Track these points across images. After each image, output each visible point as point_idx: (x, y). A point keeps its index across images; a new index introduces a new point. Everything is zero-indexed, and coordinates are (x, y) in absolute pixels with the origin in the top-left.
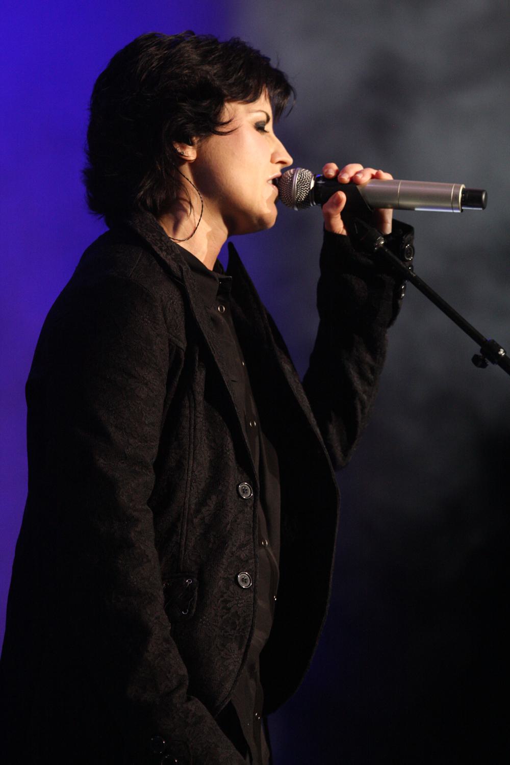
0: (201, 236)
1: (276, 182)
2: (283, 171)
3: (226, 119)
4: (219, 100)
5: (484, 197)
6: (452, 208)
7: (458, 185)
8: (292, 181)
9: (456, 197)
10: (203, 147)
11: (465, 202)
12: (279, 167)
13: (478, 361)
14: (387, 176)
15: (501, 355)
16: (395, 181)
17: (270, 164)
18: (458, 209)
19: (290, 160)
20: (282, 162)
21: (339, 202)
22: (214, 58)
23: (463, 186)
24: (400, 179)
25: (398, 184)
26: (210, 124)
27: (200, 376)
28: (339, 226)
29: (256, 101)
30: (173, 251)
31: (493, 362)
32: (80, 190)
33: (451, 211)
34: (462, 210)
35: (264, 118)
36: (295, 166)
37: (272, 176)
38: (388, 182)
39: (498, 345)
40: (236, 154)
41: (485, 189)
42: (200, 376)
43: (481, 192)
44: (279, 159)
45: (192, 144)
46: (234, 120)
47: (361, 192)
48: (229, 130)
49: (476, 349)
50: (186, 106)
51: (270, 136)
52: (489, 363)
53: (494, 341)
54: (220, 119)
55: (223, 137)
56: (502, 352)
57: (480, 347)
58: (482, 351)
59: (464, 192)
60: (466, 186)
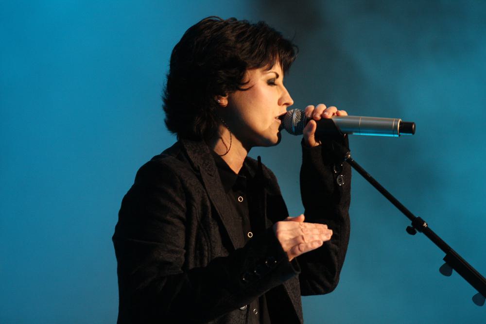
0: (234, 154)
1: (281, 117)
2: (288, 109)
3: (246, 81)
5: (413, 126)
6: (393, 134)
7: (397, 119)
8: (292, 117)
12: (285, 107)
14: (343, 113)
17: (278, 106)
19: (292, 102)
20: (286, 104)
21: (312, 126)
23: (400, 120)
25: (359, 119)
26: (237, 82)
27: (215, 231)
28: (313, 142)
31: (420, 231)
32: (162, 115)
34: (400, 135)
35: (273, 75)
37: (278, 114)
40: (252, 102)
42: (215, 231)
44: (284, 103)
45: (225, 96)
48: (247, 88)
49: (409, 223)
50: (222, 72)
54: (274, 141)
56: (425, 225)
58: (412, 224)
59: (401, 123)
60: (402, 119)
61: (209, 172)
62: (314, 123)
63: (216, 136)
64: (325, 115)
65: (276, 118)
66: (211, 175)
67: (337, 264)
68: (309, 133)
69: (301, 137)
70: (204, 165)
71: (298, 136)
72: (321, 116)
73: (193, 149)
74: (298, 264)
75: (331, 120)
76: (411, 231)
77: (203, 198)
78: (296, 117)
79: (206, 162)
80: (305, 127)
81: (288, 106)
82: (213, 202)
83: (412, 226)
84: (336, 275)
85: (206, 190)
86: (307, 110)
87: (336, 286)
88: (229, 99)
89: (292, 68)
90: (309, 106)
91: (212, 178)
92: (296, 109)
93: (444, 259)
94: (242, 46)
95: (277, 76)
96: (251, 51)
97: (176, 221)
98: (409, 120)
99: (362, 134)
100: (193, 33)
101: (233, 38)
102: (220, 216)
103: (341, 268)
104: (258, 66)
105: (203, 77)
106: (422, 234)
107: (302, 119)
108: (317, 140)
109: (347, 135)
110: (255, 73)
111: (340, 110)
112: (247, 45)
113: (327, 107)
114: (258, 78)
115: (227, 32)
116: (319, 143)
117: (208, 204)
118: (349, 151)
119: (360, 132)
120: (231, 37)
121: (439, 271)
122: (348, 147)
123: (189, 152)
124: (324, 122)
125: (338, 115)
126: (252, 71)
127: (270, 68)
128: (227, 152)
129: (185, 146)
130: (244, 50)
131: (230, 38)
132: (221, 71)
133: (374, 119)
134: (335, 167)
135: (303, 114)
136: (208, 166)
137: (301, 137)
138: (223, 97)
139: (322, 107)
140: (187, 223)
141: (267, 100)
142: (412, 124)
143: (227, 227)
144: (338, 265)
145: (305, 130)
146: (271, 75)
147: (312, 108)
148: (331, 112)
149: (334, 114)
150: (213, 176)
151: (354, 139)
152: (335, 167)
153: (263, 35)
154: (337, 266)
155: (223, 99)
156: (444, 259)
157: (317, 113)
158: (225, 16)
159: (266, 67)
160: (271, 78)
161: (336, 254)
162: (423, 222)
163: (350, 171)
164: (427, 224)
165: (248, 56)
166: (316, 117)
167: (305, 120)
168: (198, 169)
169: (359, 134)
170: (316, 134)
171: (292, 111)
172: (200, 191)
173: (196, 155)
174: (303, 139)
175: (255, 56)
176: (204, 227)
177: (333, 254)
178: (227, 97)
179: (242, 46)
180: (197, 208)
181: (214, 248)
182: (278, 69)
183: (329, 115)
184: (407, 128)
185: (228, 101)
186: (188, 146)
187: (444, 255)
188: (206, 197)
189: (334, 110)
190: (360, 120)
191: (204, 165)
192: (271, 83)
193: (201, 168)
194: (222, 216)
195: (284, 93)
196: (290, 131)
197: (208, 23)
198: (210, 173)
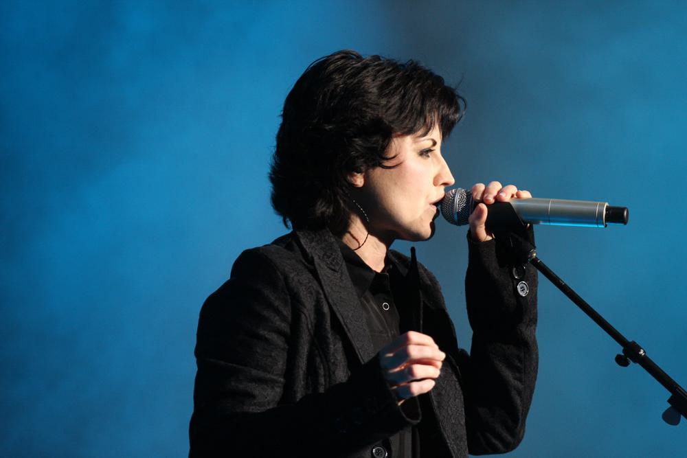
0: (373, 253)
2: (446, 190)
3: (392, 155)
4: (387, 134)
6: (597, 224)
7: (602, 203)
9: (601, 214)
12: (443, 187)
14: (526, 195)
15: (641, 355)
18: (603, 224)
19: (452, 181)
20: (445, 184)
21: (481, 212)
23: (606, 204)
26: (378, 156)
29: (415, 232)
30: (325, 240)
31: (635, 362)
32: (267, 188)
34: (606, 226)
35: (430, 143)
38: (527, 200)
39: (639, 346)
40: (398, 183)
41: (627, 206)
42: (336, 349)
49: (619, 349)
50: (358, 141)
51: (436, 156)
52: (632, 363)
53: (634, 343)
56: (642, 352)
58: (624, 351)
62: (484, 207)
63: (344, 228)
64: (499, 196)
65: (430, 204)
67: (520, 408)
68: (477, 222)
69: (466, 228)
70: (325, 257)
71: (462, 227)
72: (496, 198)
73: (309, 237)
74: (419, 409)
75: (508, 204)
76: (671, 417)
77: (318, 302)
78: (459, 200)
79: (328, 254)
80: (472, 213)
81: (447, 186)
82: (334, 308)
83: (623, 354)
84: (520, 425)
85: (323, 290)
86: (475, 189)
87: (519, 441)
88: (367, 179)
89: (455, 130)
90: (478, 185)
92: (459, 189)
93: (669, 401)
94: (388, 102)
95: (435, 143)
96: (401, 109)
97: (274, 337)
98: (618, 204)
99: (552, 224)
101: (375, 90)
102: (345, 327)
103: (526, 414)
104: (410, 131)
105: (327, 140)
106: (638, 366)
107: (468, 202)
108: (488, 232)
109: (531, 226)
110: (404, 140)
111: (522, 190)
112: (396, 99)
113: (503, 186)
114: (406, 147)
115: (366, 80)
116: (492, 236)
117: (326, 309)
118: (535, 247)
119: (549, 221)
120: (371, 85)
121: (661, 418)
122: (534, 242)
123: (303, 241)
124: (499, 207)
125: (518, 196)
127: (425, 134)
128: (360, 247)
130: (390, 108)
131: (370, 90)
132: (357, 139)
133: (561, 202)
134: (514, 269)
135: (469, 195)
136: (330, 259)
137: (466, 228)
139: (496, 186)
140: (292, 342)
141: (418, 180)
142: (623, 209)
143: (357, 344)
144: (523, 410)
145: (472, 217)
146: (426, 143)
147: (481, 187)
148: (509, 194)
149: (512, 196)
150: (338, 272)
151: (541, 231)
152: (514, 269)
153: (418, 85)
154: (521, 412)
156: (669, 401)
157: (490, 193)
158: (366, 52)
159: (420, 133)
161: (519, 393)
162: (639, 348)
163: (535, 276)
164: (644, 352)
165: (395, 117)
166: (487, 200)
167: (472, 204)
169: (548, 224)
170: (486, 224)
171: (454, 190)
172: (313, 292)
173: (313, 244)
174: (469, 231)
175: (406, 117)
176: (319, 341)
177: (514, 393)
179: (388, 102)
180: (307, 315)
181: (334, 373)
182: (436, 134)
183: (506, 197)
184: (616, 215)
185: (365, 180)
187: (669, 395)
188: (323, 300)
189: (512, 189)
190: (551, 204)
191: (325, 257)
192: (425, 153)
194: (347, 326)
195: (443, 167)
196: (450, 219)
197: (339, 63)
198: (333, 267)
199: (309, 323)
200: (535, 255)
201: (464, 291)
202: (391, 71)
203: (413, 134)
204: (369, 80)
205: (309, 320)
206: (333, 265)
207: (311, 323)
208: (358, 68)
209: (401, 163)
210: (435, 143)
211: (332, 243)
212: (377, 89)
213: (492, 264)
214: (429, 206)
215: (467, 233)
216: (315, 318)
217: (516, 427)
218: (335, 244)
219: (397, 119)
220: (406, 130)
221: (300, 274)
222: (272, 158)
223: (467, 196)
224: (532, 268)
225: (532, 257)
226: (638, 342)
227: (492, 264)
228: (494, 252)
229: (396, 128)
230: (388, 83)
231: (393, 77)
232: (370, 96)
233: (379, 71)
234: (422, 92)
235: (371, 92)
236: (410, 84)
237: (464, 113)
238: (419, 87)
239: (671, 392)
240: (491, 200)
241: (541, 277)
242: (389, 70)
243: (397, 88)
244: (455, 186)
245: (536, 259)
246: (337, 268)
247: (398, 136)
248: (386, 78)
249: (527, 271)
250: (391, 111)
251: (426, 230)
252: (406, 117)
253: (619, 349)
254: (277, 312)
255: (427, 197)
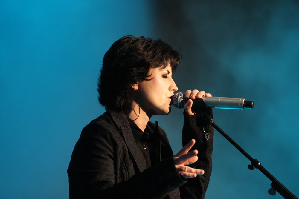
0: (141, 120)
1: (171, 98)
2: (174, 93)
3: (150, 75)
4: (147, 67)
5: (252, 103)
6: (240, 108)
8: (178, 97)
10: (141, 85)
11: (245, 106)
12: (173, 92)
13: (251, 168)
14: (209, 95)
15: (259, 165)
16: (213, 97)
18: (242, 108)
19: (177, 89)
20: (174, 90)
21: (190, 103)
22: (149, 49)
23: (244, 99)
24: (220, 97)
26: (144, 76)
28: (191, 113)
31: (256, 168)
32: (97, 95)
33: (240, 109)
34: (244, 109)
35: (167, 72)
36: (178, 91)
37: (169, 96)
38: (210, 98)
43: (251, 102)
45: (136, 84)
46: (152, 74)
47: (205, 102)
49: (249, 163)
52: (255, 168)
55: (148, 81)
56: (259, 164)
57: (251, 162)
58: (251, 163)
59: (245, 102)
61: (126, 130)
63: (129, 109)
64: (198, 96)
66: (127, 132)
67: (203, 188)
68: (188, 107)
69: (183, 110)
70: (123, 126)
72: (196, 97)
73: (116, 116)
75: (201, 99)
76: (251, 168)
78: (180, 97)
80: (186, 103)
82: (129, 149)
83: (251, 165)
86: (187, 93)
88: (139, 86)
91: (128, 134)
92: (180, 93)
95: (169, 73)
96: (153, 57)
99: (220, 108)
100: (117, 45)
101: (142, 49)
103: (206, 190)
105: (122, 73)
108: (193, 111)
112: (151, 53)
114: (157, 73)
115: (138, 45)
116: (194, 113)
119: (219, 107)
120: (141, 47)
121: (276, 195)
122: (212, 116)
124: (197, 101)
125: (206, 96)
126: (153, 69)
127: (165, 67)
128: (137, 118)
129: (111, 114)
130: (149, 56)
132: (134, 68)
134: (204, 128)
135: (184, 96)
136: (125, 127)
137: (183, 110)
138: (135, 85)
139: (196, 91)
141: (162, 87)
144: (204, 189)
145: (186, 105)
146: (165, 72)
148: (202, 95)
149: (203, 96)
152: (204, 128)
153: (161, 47)
155: (135, 86)
157: (193, 95)
158: (137, 35)
159: (162, 67)
160: (165, 73)
162: (258, 162)
164: (260, 164)
165: (151, 60)
166: (192, 98)
167: (186, 99)
168: (120, 128)
173: (118, 119)
175: (156, 60)
177: (201, 181)
178: (138, 84)
179: (148, 53)
182: (169, 68)
183: (200, 96)
184: (248, 104)
186: (113, 114)
187: (271, 182)
189: (203, 93)
190: (220, 99)
192: (165, 76)
193: (122, 127)
198: (127, 131)
199: (120, 154)
200: (213, 121)
201: (181, 137)
202: (149, 42)
203: (159, 67)
204: (140, 45)
205: (120, 153)
206: (127, 130)
207: (121, 154)
208: (134, 41)
209: (153, 78)
210: (169, 73)
211: (126, 119)
212: (143, 48)
213: (194, 124)
214: (168, 99)
215: (183, 111)
216: (185, 175)
217: (201, 196)
218: (127, 120)
219: (152, 61)
220: (156, 65)
221: (115, 133)
222: (98, 80)
223: (183, 96)
224: (212, 127)
225: (212, 122)
226: (258, 159)
227: (194, 124)
228: (195, 120)
229: (152, 64)
230: (148, 46)
231: (150, 44)
232: (140, 51)
233: (144, 41)
234: (162, 52)
235: (140, 49)
236: (157, 47)
237: (181, 61)
238: (161, 48)
239: (272, 181)
240: (194, 98)
241: (216, 132)
242: (148, 41)
243: (152, 48)
244: (178, 91)
245: (214, 123)
246: (128, 131)
247: (152, 68)
248: (147, 44)
249: (209, 129)
250: (149, 57)
251: (166, 109)
252: (156, 60)
253: (249, 163)
254: (110, 149)
255: (166, 95)
